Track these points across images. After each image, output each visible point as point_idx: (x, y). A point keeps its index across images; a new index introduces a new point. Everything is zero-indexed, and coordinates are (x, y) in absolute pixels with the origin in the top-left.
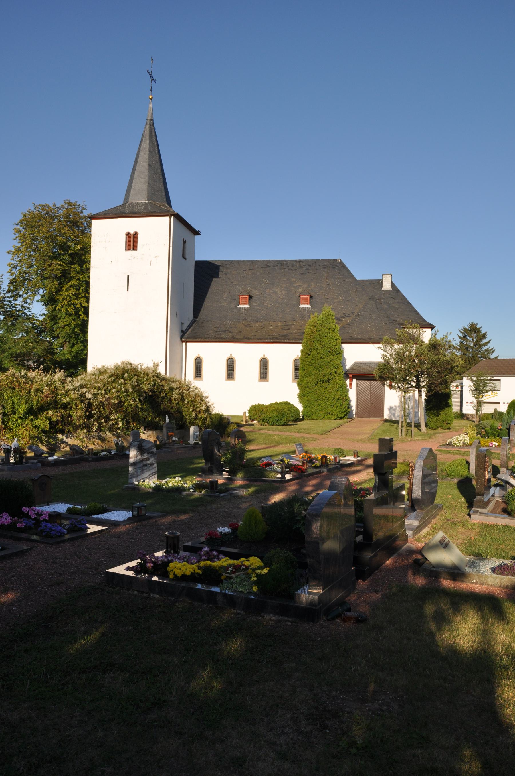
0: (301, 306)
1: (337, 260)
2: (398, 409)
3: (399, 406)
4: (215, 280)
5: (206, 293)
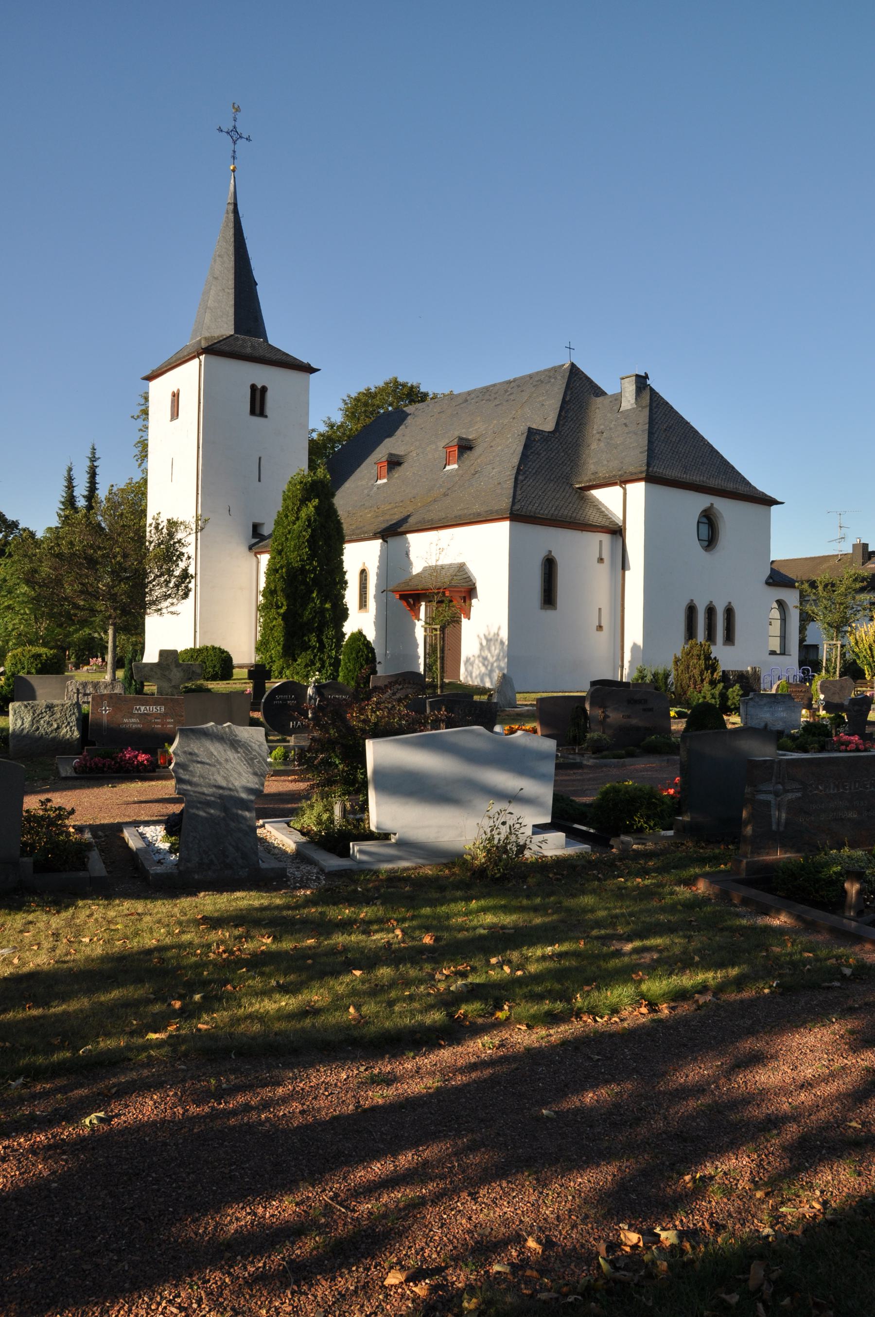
0: (448, 468)
1: (563, 365)
2: (477, 661)
3: (479, 657)
4: (387, 440)
5: (359, 466)
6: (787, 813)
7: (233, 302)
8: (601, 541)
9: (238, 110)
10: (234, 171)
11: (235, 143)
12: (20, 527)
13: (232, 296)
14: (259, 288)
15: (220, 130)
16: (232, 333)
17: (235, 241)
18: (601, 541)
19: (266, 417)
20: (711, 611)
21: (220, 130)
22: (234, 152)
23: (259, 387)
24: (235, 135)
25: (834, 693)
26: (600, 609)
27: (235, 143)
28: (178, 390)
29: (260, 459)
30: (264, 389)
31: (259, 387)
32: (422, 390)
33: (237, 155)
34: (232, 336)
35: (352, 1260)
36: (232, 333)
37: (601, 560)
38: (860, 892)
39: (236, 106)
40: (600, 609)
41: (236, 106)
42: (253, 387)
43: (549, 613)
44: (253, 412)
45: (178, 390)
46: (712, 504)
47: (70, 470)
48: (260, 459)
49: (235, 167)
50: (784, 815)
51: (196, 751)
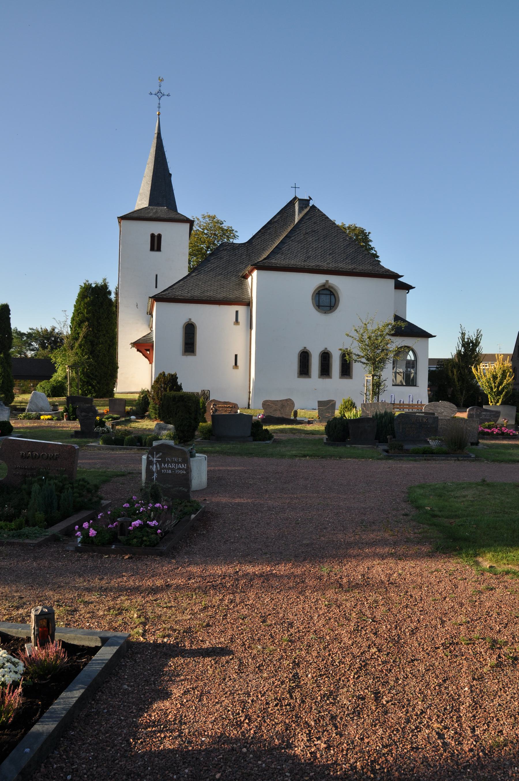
7: (150, 189)
8: (237, 312)
9: (162, 80)
14: (173, 179)
15: (151, 94)
18: (237, 312)
20: (326, 357)
21: (151, 94)
23: (156, 234)
24: (160, 94)
25: (275, 410)
26: (236, 356)
29: (157, 276)
30: (159, 236)
32: (347, 226)
33: (161, 105)
35: (326, 773)
37: (237, 322)
39: (161, 78)
40: (236, 356)
41: (161, 78)
42: (153, 236)
43: (190, 358)
44: (152, 249)
46: (327, 281)
49: (159, 113)
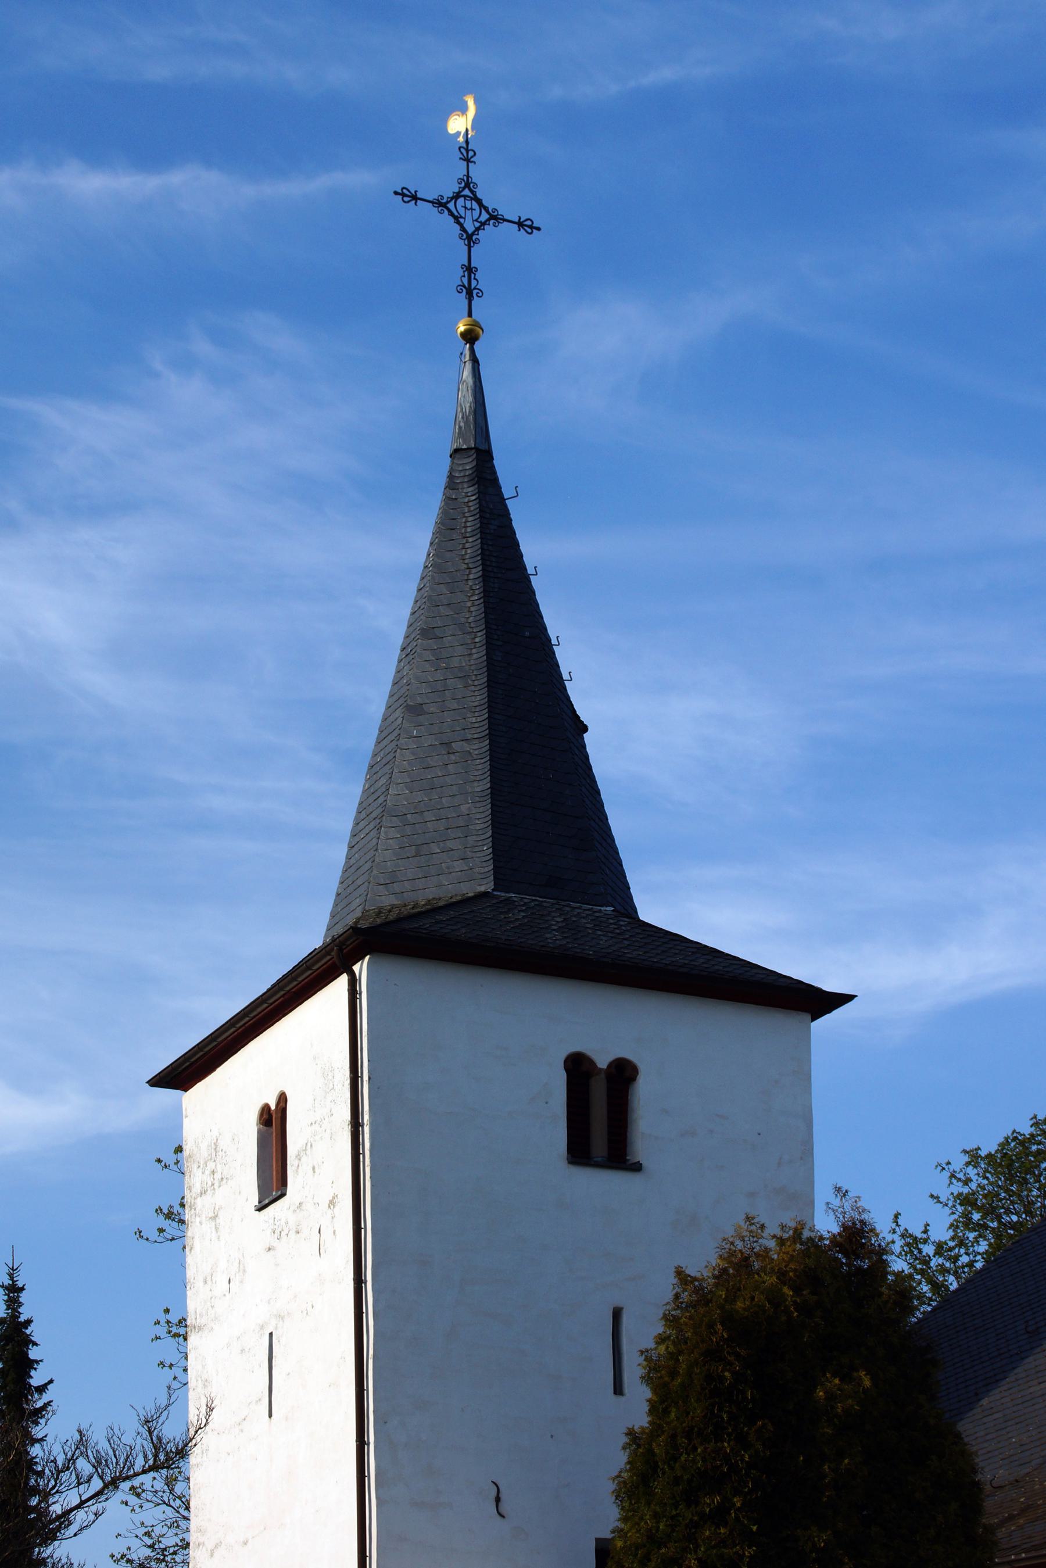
6: (719, 1496)
7: (483, 785)
10: (470, 337)
11: (470, 239)
12: (958, 1170)
13: (481, 768)
16: (487, 886)
17: (486, 577)
19: (637, 1168)
22: (470, 270)
23: (602, 1062)
27: (470, 239)
28: (282, 1099)
29: (617, 1314)
31: (602, 1062)
33: (483, 280)
34: (485, 894)
36: (487, 886)
38: (752, 1529)
45: (282, 1099)
47: (51, 1381)
48: (617, 1314)
50: (718, 1498)
51: (450, 491)
